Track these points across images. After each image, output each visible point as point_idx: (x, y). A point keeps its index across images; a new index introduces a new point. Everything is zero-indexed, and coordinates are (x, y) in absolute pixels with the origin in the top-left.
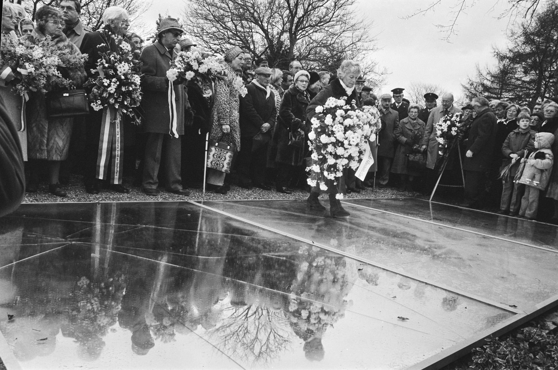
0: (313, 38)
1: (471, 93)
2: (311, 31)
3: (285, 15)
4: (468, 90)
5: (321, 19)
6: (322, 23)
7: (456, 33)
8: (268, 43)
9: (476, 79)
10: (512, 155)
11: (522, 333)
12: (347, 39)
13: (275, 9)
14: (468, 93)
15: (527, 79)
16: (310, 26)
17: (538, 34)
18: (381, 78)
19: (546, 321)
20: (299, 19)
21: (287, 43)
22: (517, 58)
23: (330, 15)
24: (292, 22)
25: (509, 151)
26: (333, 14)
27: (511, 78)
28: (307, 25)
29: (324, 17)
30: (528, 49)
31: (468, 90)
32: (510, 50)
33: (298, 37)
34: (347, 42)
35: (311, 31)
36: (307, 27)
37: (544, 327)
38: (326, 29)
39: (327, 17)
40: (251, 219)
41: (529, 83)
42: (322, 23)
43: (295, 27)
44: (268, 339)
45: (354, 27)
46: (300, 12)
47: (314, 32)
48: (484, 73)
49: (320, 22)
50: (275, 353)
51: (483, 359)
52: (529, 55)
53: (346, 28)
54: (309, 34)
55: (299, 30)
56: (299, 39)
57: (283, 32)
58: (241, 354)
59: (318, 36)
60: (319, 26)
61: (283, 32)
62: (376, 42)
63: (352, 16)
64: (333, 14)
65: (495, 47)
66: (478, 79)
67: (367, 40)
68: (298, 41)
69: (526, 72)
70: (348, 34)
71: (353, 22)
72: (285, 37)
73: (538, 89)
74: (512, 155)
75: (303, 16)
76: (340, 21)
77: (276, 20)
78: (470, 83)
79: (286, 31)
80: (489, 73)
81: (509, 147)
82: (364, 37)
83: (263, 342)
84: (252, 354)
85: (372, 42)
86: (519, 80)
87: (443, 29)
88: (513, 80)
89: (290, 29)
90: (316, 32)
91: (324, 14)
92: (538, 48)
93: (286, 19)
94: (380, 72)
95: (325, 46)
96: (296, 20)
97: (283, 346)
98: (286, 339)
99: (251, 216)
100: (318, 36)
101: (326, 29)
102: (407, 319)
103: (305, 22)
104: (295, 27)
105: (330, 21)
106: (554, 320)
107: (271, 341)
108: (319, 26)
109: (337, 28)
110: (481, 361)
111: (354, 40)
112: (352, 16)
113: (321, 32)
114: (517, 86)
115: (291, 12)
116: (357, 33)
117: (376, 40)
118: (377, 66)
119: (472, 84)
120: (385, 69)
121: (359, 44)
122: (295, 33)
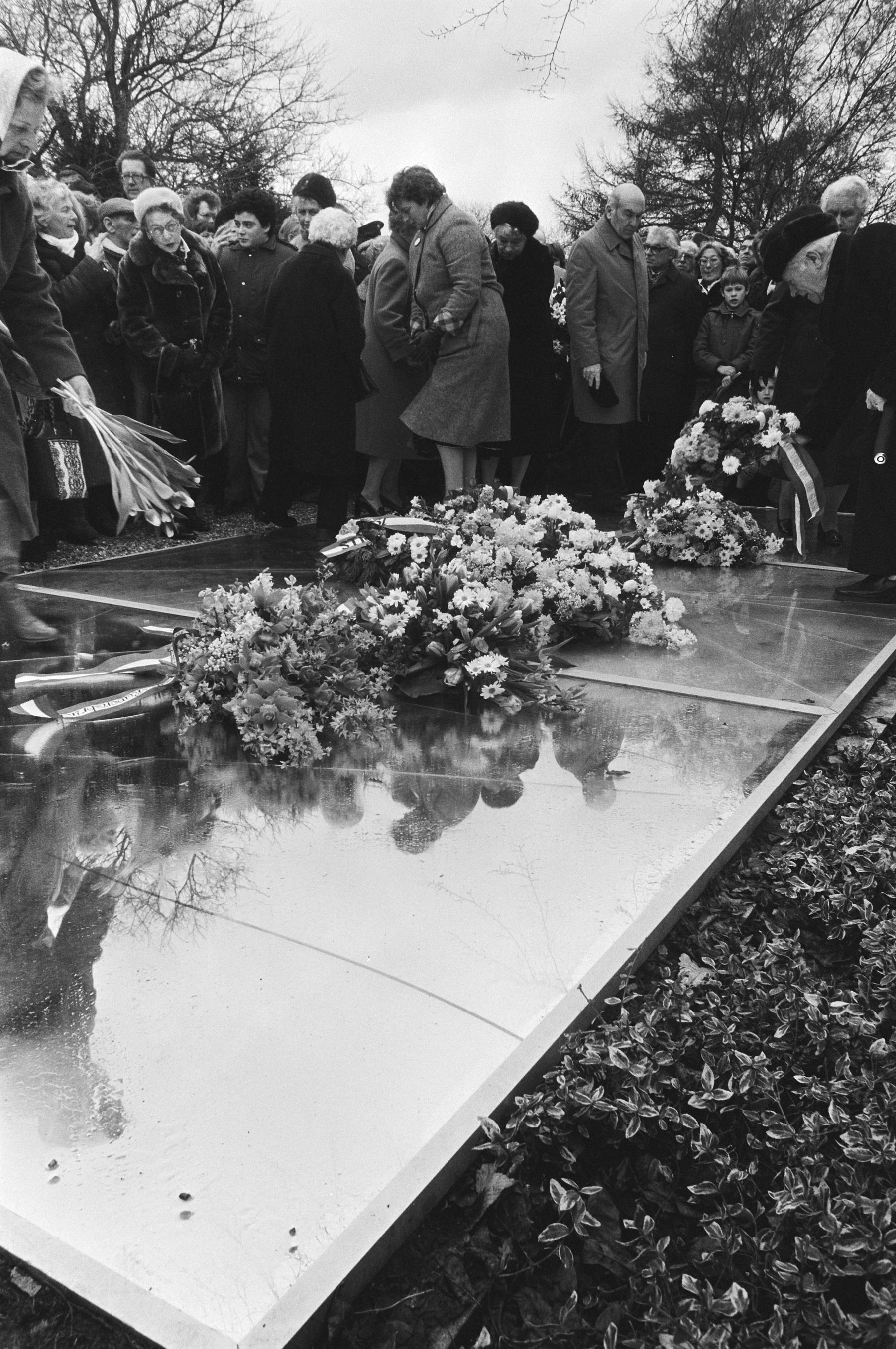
0: (179, 96)
1: (574, 217)
2: (168, 76)
3: (84, 29)
4: (567, 210)
5: (188, 40)
6: (194, 53)
7: (561, 73)
8: (54, 118)
9: (582, 184)
10: (722, 369)
11: (836, 753)
12: (264, 98)
13: (54, 14)
14: (568, 220)
15: (692, 175)
16: (161, 61)
17: (705, 63)
18: (360, 196)
19: (865, 719)
20: (130, 40)
21: (108, 113)
22: (669, 126)
23: (213, 27)
24: (108, 48)
25: (717, 360)
26: (221, 23)
27: (658, 176)
28: (152, 60)
29: (197, 33)
30: (686, 101)
31: (567, 210)
32: (649, 107)
33: (134, 94)
34: (266, 105)
35: (168, 76)
36: (154, 65)
37: (864, 733)
38: (207, 68)
39: (203, 36)
40: (167, 602)
41: (696, 184)
42: (194, 53)
43: (123, 68)
44: (190, 876)
45: (281, 62)
46: (128, 24)
47: (175, 78)
48: (599, 167)
49: (188, 48)
50: (213, 900)
51: (805, 824)
52: (694, 116)
53: (258, 63)
54: (164, 85)
55: (135, 75)
56: (137, 100)
57: (88, 80)
58: (130, 920)
59: (188, 90)
60: (188, 61)
61: (88, 80)
62: (341, 99)
63: (270, 29)
64: (221, 23)
65: (615, 103)
66: (587, 181)
67: (318, 95)
68: (139, 107)
69: (687, 161)
70: (265, 81)
71: (275, 46)
72: (98, 96)
73: (716, 199)
74: (722, 369)
75: (138, 35)
76: (244, 45)
77: (65, 45)
78: (572, 192)
79: (96, 79)
80: (610, 168)
81: (710, 347)
82: (310, 87)
83: (180, 885)
84: (157, 917)
85: (333, 100)
86: (676, 180)
87: (532, 63)
88: (664, 182)
89: (109, 75)
90: (181, 78)
91: (194, 24)
92: (708, 97)
93: (90, 43)
94: (356, 180)
95: (213, 119)
96: (119, 44)
97: (230, 880)
98: (233, 866)
99: (162, 594)
100: (188, 90)
101: (207, 68)
102: (627, 772)
103: (145, 51)
104: (123, 68)
105: (213, 47)
106: (878, 714)
107: (199, 877)
108: (188, 61)
109: (236, 64)
110: (802, 827)
111: (285, 96)
112: (270, 29)
113: (195, 77)
114: (673, 195)
115: (101, 20)
116: (294, 77)
117: (341, 94)
118: (346, 165)
119: (575, 197)
120: (369, 171)
121: (299, 107)
122: (124, 84)
